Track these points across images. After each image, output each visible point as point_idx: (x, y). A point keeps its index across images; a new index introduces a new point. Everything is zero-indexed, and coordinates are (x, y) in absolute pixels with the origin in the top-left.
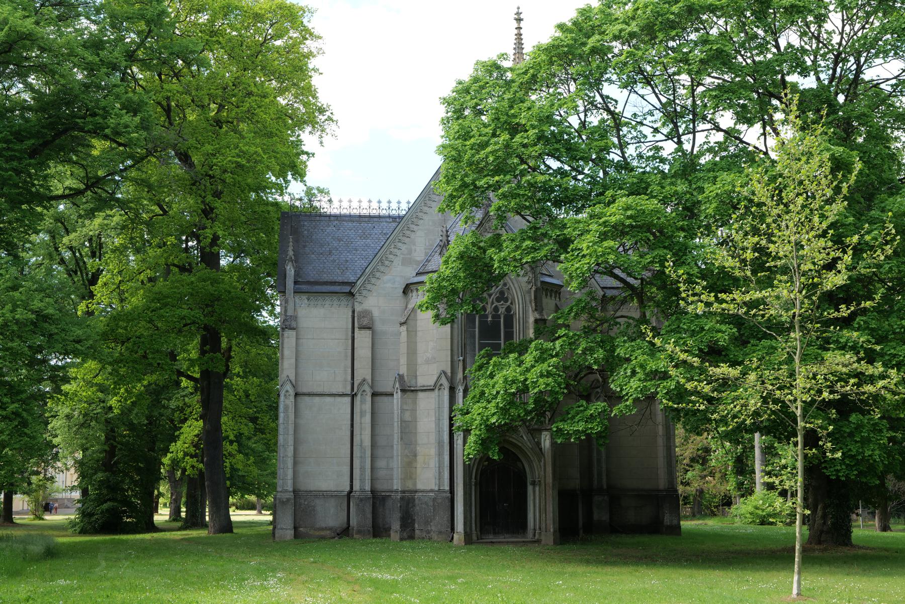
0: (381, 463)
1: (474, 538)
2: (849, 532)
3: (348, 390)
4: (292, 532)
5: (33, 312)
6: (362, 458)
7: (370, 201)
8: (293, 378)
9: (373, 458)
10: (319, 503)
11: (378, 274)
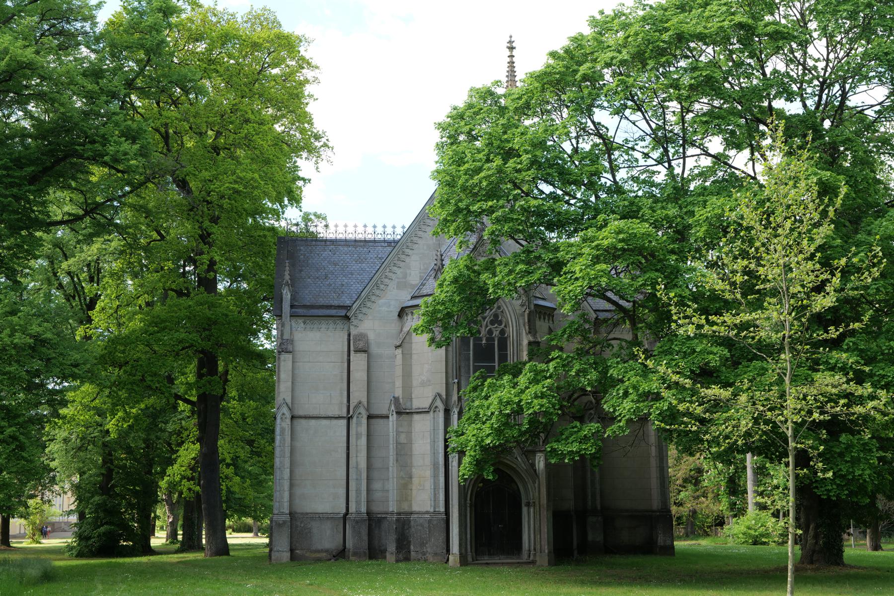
0: (377, 485)
1: (470, 559)
2: (840, 551)
3: (344, 413)
4: (289, 554)
5: (31, 336)
6: (358, 480)
7: (365, 226)
8: (289, 401)
9: (369, 480)
10: (315, 526)
11: (373, 298)
